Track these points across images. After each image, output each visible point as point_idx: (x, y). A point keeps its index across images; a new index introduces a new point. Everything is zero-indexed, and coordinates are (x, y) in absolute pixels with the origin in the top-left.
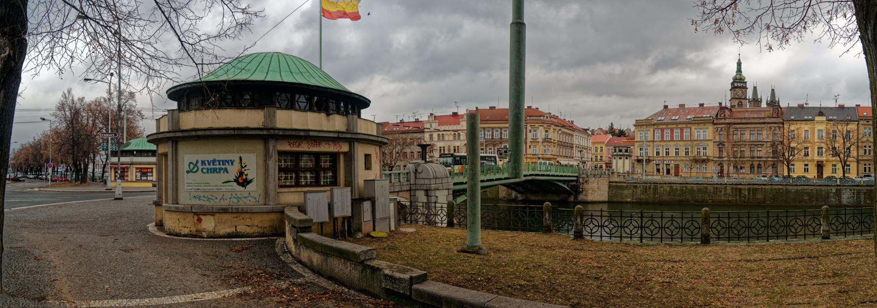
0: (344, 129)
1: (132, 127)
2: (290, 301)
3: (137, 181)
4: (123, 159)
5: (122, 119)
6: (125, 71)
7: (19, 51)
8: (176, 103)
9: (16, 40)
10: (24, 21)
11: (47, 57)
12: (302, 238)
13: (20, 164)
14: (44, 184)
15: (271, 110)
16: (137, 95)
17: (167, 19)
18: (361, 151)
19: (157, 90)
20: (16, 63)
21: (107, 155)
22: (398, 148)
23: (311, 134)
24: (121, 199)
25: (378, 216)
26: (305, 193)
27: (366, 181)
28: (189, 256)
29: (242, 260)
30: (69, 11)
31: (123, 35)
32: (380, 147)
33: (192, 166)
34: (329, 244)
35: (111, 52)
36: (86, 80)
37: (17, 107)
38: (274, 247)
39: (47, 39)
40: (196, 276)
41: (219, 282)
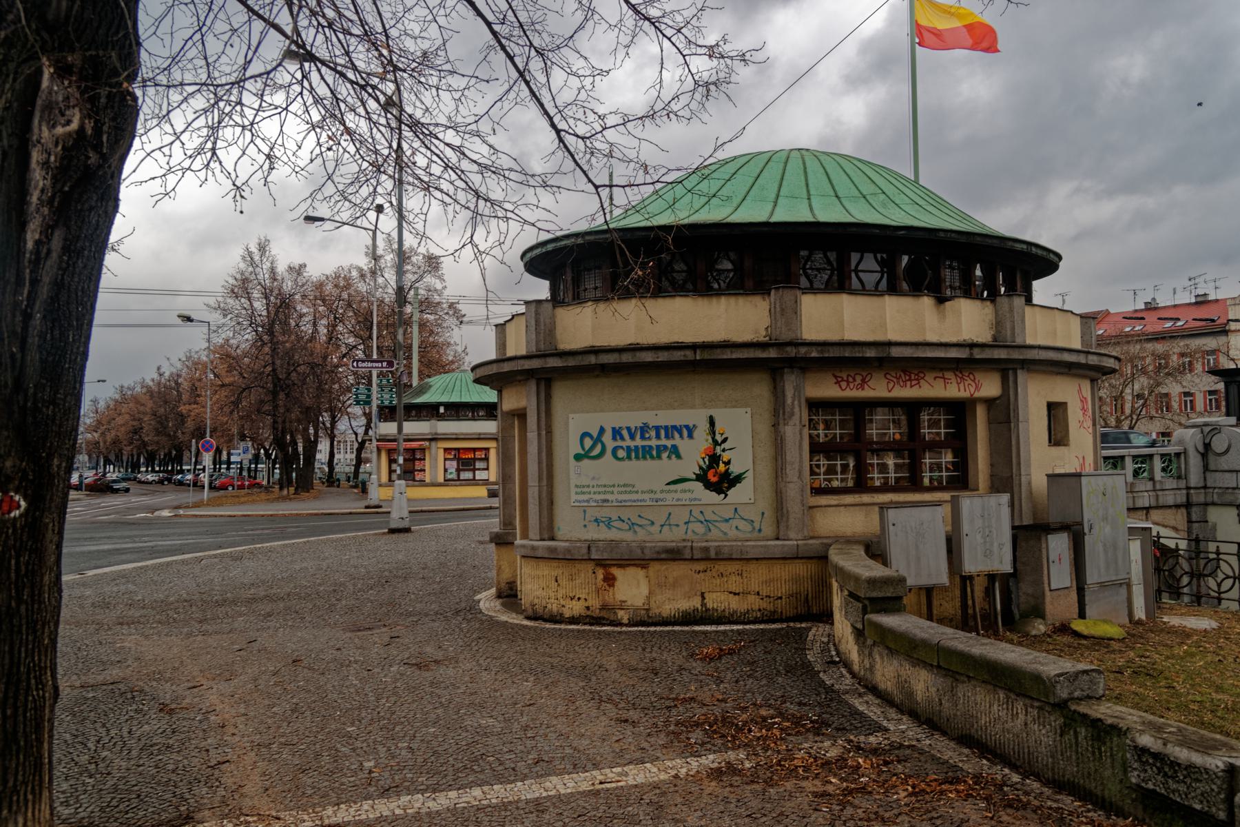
0: (985, 336)
1: (434, 345)
2: (851, 792)
3: (447, 482)
4: (411, 427)
5: (407, 323)
6: (414, 201)
7: (113, 127)
8: (546, 284)
9: (104, 92)
10: (129, 47)
11: (200, 151)
12: (879, 628)
13: (116, 442)
14: (190, 496)
15: (788, 295)
16: (447, 264)
17: (521, 74)
18: (1035, 395)
19: (497, 252)
20: (104, 157)
21: (368, 416)
22: (1141, 383)
23: (896, 352)
24: (407, 530)
25: (1092, 577)
26: (883, 507)
27: (1052, 477)
28: (585, 673)
29: (719, 681)
30: (263, 35)
31: (409, 109)
32: (1093, 381)
33: (588, 443)
34: (961, 647)
35: (376, 152)
36: (310, 219)
37: (106, 280)
38: (802, 650)
39: (199, 102)
40: (601, 725)
41: (662, 739)
